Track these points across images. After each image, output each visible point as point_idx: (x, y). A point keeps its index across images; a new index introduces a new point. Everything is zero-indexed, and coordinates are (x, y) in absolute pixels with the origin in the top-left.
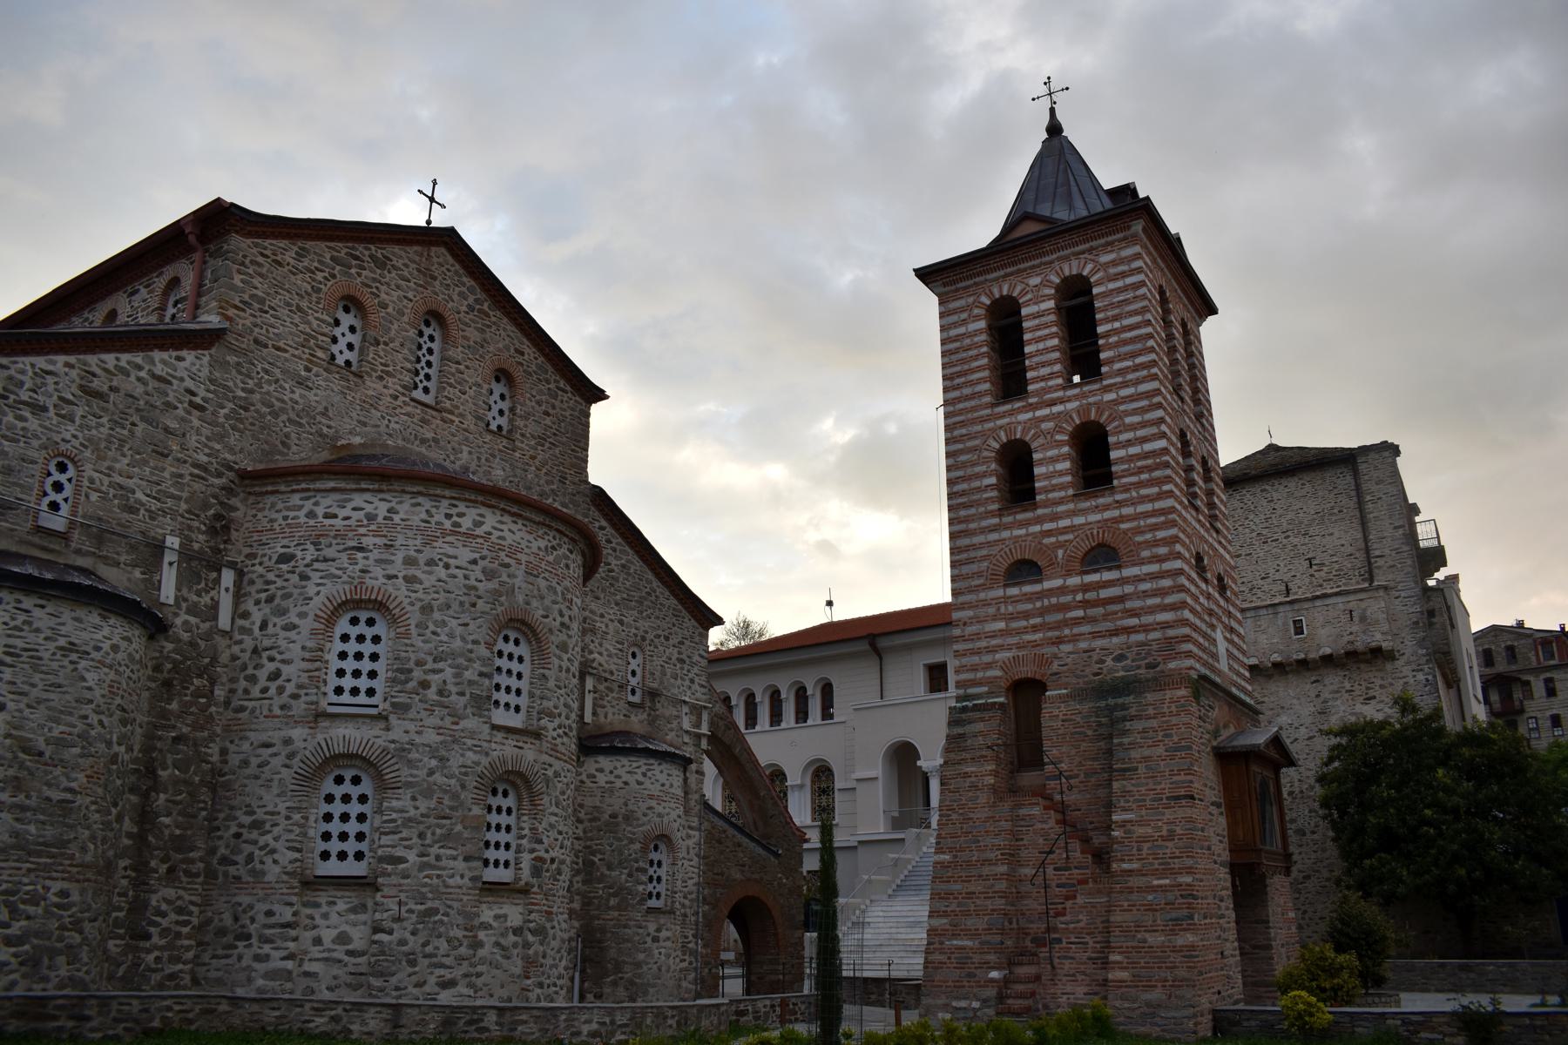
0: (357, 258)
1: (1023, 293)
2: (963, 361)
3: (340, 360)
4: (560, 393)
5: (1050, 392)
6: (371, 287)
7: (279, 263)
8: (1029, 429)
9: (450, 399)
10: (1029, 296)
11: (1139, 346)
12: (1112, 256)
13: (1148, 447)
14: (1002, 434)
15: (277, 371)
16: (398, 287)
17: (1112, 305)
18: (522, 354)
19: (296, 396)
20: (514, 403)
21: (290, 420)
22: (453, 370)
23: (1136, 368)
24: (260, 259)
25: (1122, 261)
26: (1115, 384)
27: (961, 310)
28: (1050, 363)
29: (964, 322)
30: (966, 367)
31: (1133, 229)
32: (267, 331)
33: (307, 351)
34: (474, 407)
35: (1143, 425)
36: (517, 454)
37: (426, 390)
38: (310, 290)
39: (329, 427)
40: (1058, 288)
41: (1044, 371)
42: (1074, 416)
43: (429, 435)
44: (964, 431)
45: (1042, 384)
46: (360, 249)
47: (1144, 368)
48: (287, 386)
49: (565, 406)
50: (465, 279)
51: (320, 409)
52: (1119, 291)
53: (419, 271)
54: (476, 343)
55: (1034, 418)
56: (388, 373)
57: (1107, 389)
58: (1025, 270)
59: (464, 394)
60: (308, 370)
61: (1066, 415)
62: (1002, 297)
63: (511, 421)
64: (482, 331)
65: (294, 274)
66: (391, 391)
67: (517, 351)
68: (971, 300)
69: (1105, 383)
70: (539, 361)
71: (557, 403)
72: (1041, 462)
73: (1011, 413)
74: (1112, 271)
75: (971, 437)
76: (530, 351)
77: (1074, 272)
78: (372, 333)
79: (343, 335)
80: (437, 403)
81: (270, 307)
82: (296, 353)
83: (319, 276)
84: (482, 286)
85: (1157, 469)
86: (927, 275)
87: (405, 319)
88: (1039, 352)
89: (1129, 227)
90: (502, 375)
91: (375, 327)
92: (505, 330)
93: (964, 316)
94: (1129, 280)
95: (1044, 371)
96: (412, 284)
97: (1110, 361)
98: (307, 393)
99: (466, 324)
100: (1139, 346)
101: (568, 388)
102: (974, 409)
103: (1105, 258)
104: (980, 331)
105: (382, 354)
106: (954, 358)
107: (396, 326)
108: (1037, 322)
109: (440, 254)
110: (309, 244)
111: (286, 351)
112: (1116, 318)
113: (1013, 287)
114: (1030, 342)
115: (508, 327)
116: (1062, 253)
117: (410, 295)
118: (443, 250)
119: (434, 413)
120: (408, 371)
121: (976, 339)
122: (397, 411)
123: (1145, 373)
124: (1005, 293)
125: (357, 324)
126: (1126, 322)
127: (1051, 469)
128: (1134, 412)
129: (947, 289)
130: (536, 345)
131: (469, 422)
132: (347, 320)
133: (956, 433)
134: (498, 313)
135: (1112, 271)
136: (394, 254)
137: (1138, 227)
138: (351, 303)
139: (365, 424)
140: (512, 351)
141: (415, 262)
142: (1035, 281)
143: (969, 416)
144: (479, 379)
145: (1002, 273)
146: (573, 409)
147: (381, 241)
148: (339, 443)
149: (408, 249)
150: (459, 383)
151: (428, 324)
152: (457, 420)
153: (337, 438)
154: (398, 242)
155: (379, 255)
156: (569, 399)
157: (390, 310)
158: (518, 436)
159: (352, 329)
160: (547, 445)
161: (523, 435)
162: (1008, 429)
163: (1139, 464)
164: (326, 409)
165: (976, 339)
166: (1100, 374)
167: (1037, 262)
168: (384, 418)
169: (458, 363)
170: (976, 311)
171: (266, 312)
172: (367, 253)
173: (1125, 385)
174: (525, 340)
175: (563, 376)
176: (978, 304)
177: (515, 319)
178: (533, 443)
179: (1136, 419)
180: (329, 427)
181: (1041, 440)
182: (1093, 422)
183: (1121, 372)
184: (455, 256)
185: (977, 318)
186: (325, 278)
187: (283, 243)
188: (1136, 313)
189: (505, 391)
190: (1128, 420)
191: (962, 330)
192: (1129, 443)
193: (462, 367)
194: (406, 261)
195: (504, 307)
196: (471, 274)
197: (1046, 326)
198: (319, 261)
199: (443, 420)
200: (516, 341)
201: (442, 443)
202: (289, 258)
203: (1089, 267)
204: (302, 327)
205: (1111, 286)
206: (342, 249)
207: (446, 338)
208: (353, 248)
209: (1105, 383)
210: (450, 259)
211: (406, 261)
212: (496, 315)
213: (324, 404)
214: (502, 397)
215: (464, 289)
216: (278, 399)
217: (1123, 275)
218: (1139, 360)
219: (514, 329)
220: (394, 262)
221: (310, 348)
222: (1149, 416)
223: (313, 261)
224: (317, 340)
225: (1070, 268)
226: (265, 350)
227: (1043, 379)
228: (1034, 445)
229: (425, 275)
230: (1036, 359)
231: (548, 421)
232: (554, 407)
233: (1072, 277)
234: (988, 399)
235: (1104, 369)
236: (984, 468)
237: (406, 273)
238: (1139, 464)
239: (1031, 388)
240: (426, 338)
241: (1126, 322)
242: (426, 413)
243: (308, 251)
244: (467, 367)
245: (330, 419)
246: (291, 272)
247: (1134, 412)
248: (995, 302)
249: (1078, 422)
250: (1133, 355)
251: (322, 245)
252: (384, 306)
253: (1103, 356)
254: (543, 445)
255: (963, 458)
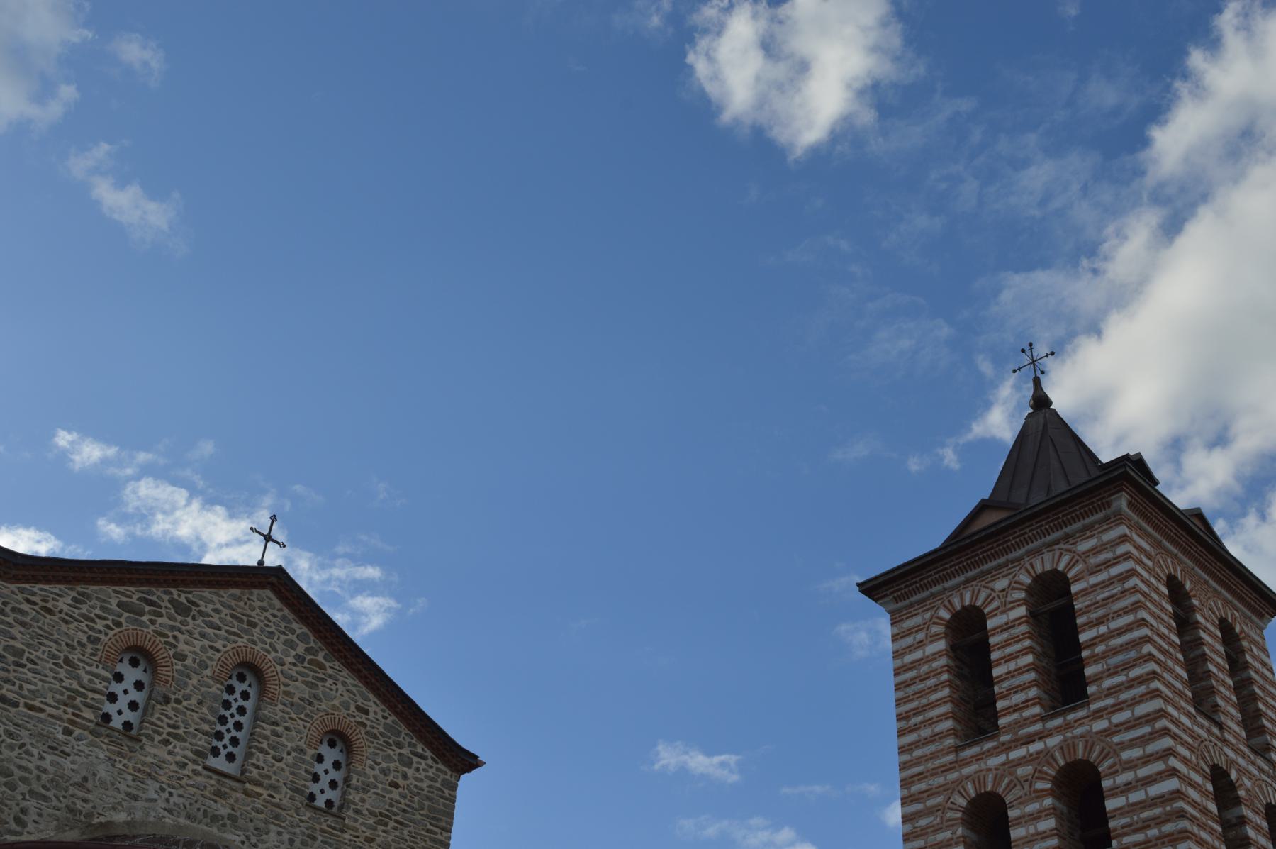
0: (151, 603)
1: (989, 600)
2: (920, 694)
3: (117, 722)
4: (415, 759)
5: (1025, 726)
6: (166, 636)
7: (49, 611)
8: (1003, 777)
9: (258, 767)
10: (995, 604)
11: (1132, 654)
12: (1092, 543)
13: (1154, 790)
14: (970, 786)
15: (24, 733)
16: (203, 635)
17: (1095, 605)
18: (367, 712)
19: (46, 764)
20: (349, 771)
21: (31, 792)
22: (268, 733)
23: (1130, 684)
24: (25, 607)
25: (1103, 548)
26: (1105, 709)
27: (917, 629)
28: (1024, 688)
29: (920, 644)
30: (924, 701)
31: (1114, 505)
32: (21, 687)
33: (70, 710)
34: (291, 777)
35: (1147, 760)
36: (347, 836)
37: (231, 757)
38: (85, 640)
39: (85, 801)
40: (1029, 590)
41: (1018, 698)
42: (1057, 755)
43: (224, 811)
44: (923, 786)
45: (1015, 716)
46: (158, 594)
47: (1141, 683)
48: (35, 752)
49: (422, 775)
50: (295, 626)
51: (77, 778)
52: (1104, 585)
53: (232, 616)
54: (302, 700)
55: (1008, 762)
56: (176, 737)
57: (1097, 715)
58: (989, 572)
59: (280, 760)
60: (68, 732)
61: (1047, 754)
62: (964, 608)
63: (344, 793)
64: (312, 685)
65: (67, 622)
66: (179, 758)
67: (358, 708)
68: (928, 615)
69: (1093, 707)
70: (389, 721)
71: (410, 772)
72: (1019, 821)
73: (979, 758)
74: (1093, 561)
75: (930, 793)
76: (376, 708)
77: (1048, 568)
78: (160, 688)
79: (126, 692)
80: (243, 772)
81: (28, 659)
82: (54, 711)
83: (100, 625)
84: (316, 632)
85: (1168, 821)
86: (873, 589)
87: (208, 672)
88: (1011, 675)
89: (1109, 505)
90: (336, 737)
91: (167, 682)
92: (344, 683)
93: (920, 636)
94: (1115, 571)
95: (1018, 698)
96: (223, 632)
97: (1098, 678)
98: (60, 760)
99: (290, 678)
100: (1132, 654)
101: (428, 753)
102: (933, 756)
103: (1084, 546)
104: (938, 654)
105: (171, 713)
106: (910, 690)
107: (194, 681)
108: (1005, 635)
109: (264, 600)
110: (91, 589)
111: (42, 711)
112: (1100, 621)
113: (975, 596)
114: (998, 662)
115: (349, 681)
116: (1031, 546)
117: (218, 645)
118: (268, 593)
119: (234, 784)
120: (206, 733)
121: (935, 665)
122: (183, 782)
123: (1142, 689)
124: (967, 602)
125: (144, 678)
126: (1114, 625)
127: (1032, 830)
128: (1133, 743)
129: (900, 604)
130: (385, 701)
131: (283, 797)
132: (132, 674)
133: (914, 789)
134: (337, 665)
135: (1093, 561)
136: (202, 598)
137: (1122, 502)
138: (139, 654)
139: (136, 798)
140: (353, 708)
141: (229, 607)
142: (1001, 584)
143: (930, 765)
144: (302, 744)
145: (961, 578)
146: (432, 779)
147: (185, 584)
148: (96, 821)
149: (222, 592)
150: (274, 748)
151: (241, 678)
152: (265, 793)
153: (89, 815)
154: (209, 585)
155: (183, 600)
156: (427, 769)
157: (189, 662)
158: (351, 813)
159: (139, 686)
160: (392, 824)
161: (357, 812)
162: (978, 779)
163: (1145, 815)
164: (85, 779)
165: (935, 665)
166: (1085, 695)
167: (1002, 560)
168: (163, 790)
169: (275, 724)
170: (934, 629)
171: (23, 666)
172: (166, 597)
173: (1118, 707)
174: (371, 696)
175: (422, 738)
176: (936, 620)
177: (359, 671)
178: (371, 821)
179: (1136, 753)
180: (85, 801)
181: (1018, 791)
182: (1081, 761)
183: (1112, 691)
184: (283, 599)
185: (935, 638)
186: (108, 627)
187: (56, 589)
188: (1126, 611)
189: (341, 757)
190: (1125, 755)
191: (918, 655)
192: (1129, 787)
193: (279, 729)
194: (219, 606)
195: (345, 657)
196: (303, 619)
197: (1018, 640)
198: (103, 608)
199: (246, 793)
200: (358, 697)
201: (241, 822)
202: (63, 604)
203: (1065, 559)
204: (67, 683)
205: (1094, 580)
206: (134, 594)
207: (262, 693)
208: (147, 593)
209: (1093, 707)
210: (277, 603)
211: (219, 606)
212: (333, 667)
213: (84, 773)
214: (337, 765)
215: (294, 638)
216: (20, 767)
217: (1107, 564)
218: (1135, 673)
219: (357, 682)
220: (202, 608)
221: (74, 707)
222: (1152, 748)
223: (94, 607)
224: (85, 696)
225: (1043, 564)
226: (13, 710)
227: (1016, 709)
228: (1008, 799)
229: (241, 621)
230: (1006, 684)
231: (395, 794)
232: (405, 776)
233: (1045, 573)
234: (950, 741)
235: (1091, 689)
236: (948, 834)
237: (216, 620)
238: (1145, 815)
239: (1002, 722)
240: (237, 695)
241: (1114, 625)
242: (223, 784)
243: (89, 597)
244: (287, 729)
245: (89, 791)
246: (64, 620)
247: (1133, 743)
248: (956, 616)
249: (1062, 763)
250: (1126, 667)
251: (109, 589)
252: (181, 657)
253: (1088, 671)
254: (386, 825)
255: (923, 822)
